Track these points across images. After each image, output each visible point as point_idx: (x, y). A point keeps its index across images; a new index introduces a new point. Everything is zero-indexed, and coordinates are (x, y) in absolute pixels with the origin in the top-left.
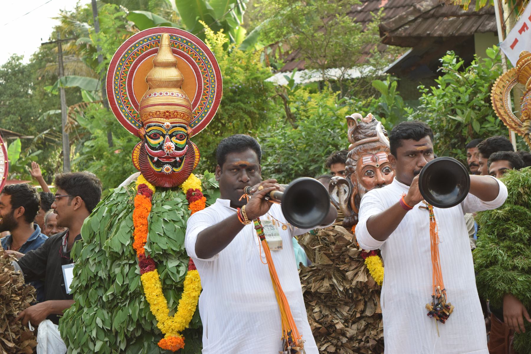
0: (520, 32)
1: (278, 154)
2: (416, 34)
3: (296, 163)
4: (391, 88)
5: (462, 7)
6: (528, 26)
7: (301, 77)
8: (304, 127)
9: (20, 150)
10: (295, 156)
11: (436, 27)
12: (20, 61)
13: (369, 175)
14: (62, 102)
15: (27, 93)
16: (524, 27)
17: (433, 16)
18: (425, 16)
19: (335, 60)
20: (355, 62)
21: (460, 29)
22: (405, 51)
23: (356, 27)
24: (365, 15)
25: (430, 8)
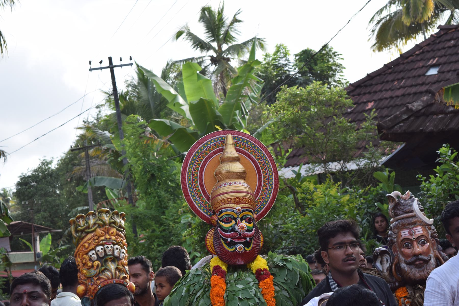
1: (292, 238)
3: (309, 246)
4: (391, 178)
7: (306, 171)
8: (314, 213)
9: (50, 243)
10: (307, 240)
11: (428, 124)
12: (50, 166)
13: (407, 247)
14: (90, 199)
15: (55, 193)
17: (424, 114)
18: (417, 114)
19: (334, 156)
21: (449, 124)
22: (401, 145)
23: (351, 126)
25: (420, 107)
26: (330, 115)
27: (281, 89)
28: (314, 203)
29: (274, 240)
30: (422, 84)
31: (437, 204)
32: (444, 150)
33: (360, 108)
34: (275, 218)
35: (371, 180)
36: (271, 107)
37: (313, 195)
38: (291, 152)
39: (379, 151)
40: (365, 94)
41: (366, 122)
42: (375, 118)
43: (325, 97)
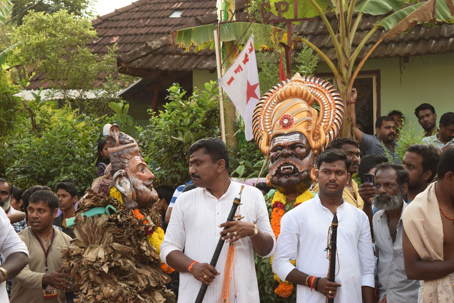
0: (236, 72)
2: (147, 66)
3: (40, 167)
5: (185, 49)
6: (242, 68)
7: (45, 95)
10: (39, 161)
16: (239, 69)
17: (161, 53)
18: (155, 52)
20: (91, 86)
21: (183, 65)
24: (99, 48)
25: (159, 46)
26: (74, 44)
27: (28, 13)
28: (50, 127)
29: (8, 158)
30: (166, 25)
31: (162, 137)
32: (174, 88)
33: (105, 41)
34: (11, 137)
35: (107, 109)
36: (17, 30)
37: (50, 119)
38: (34, 76)
39: (119, 83)
40: (111, 28)
41: (107, 54)
42: (116, 52)
43: (71, 26)
